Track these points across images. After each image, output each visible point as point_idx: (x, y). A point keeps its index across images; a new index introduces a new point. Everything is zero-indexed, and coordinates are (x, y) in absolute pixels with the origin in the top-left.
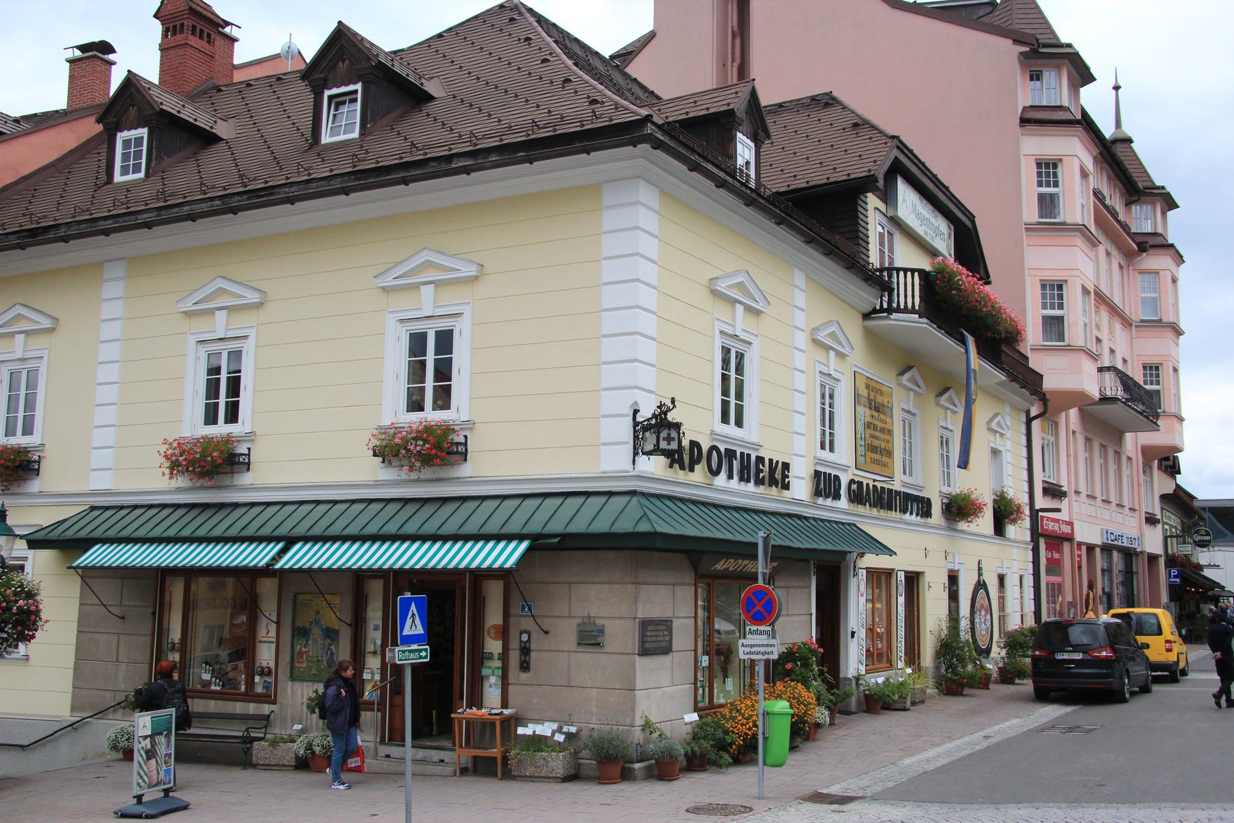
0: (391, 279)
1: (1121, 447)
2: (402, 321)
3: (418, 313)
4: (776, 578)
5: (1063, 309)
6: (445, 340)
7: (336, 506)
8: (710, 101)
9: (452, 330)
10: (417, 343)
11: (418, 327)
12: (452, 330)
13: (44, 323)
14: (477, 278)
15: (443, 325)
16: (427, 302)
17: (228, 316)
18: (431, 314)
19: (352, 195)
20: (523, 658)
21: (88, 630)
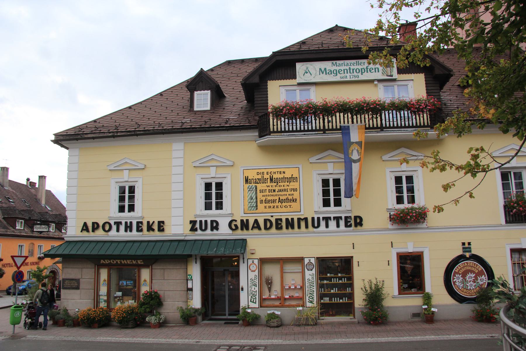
0: (113, 167)
1: (401, 267)
2: (319, 174)
3: (208, 175)
4: (111, 308)
5: (222, 209)
6: (132, 190)
7: (164, 243)
8: (163, 120)
9: (222, 183)
10: (122, 190)
11: (398, 174)
12: (340, 179)
13: (228, 163)
14: (144, 169)
15: (132, 184)
16: (213, 172)
17: (129, 171)
18: (332, 173)
19: (95, 140)
20: (115, 324)
21: (86, 280)
